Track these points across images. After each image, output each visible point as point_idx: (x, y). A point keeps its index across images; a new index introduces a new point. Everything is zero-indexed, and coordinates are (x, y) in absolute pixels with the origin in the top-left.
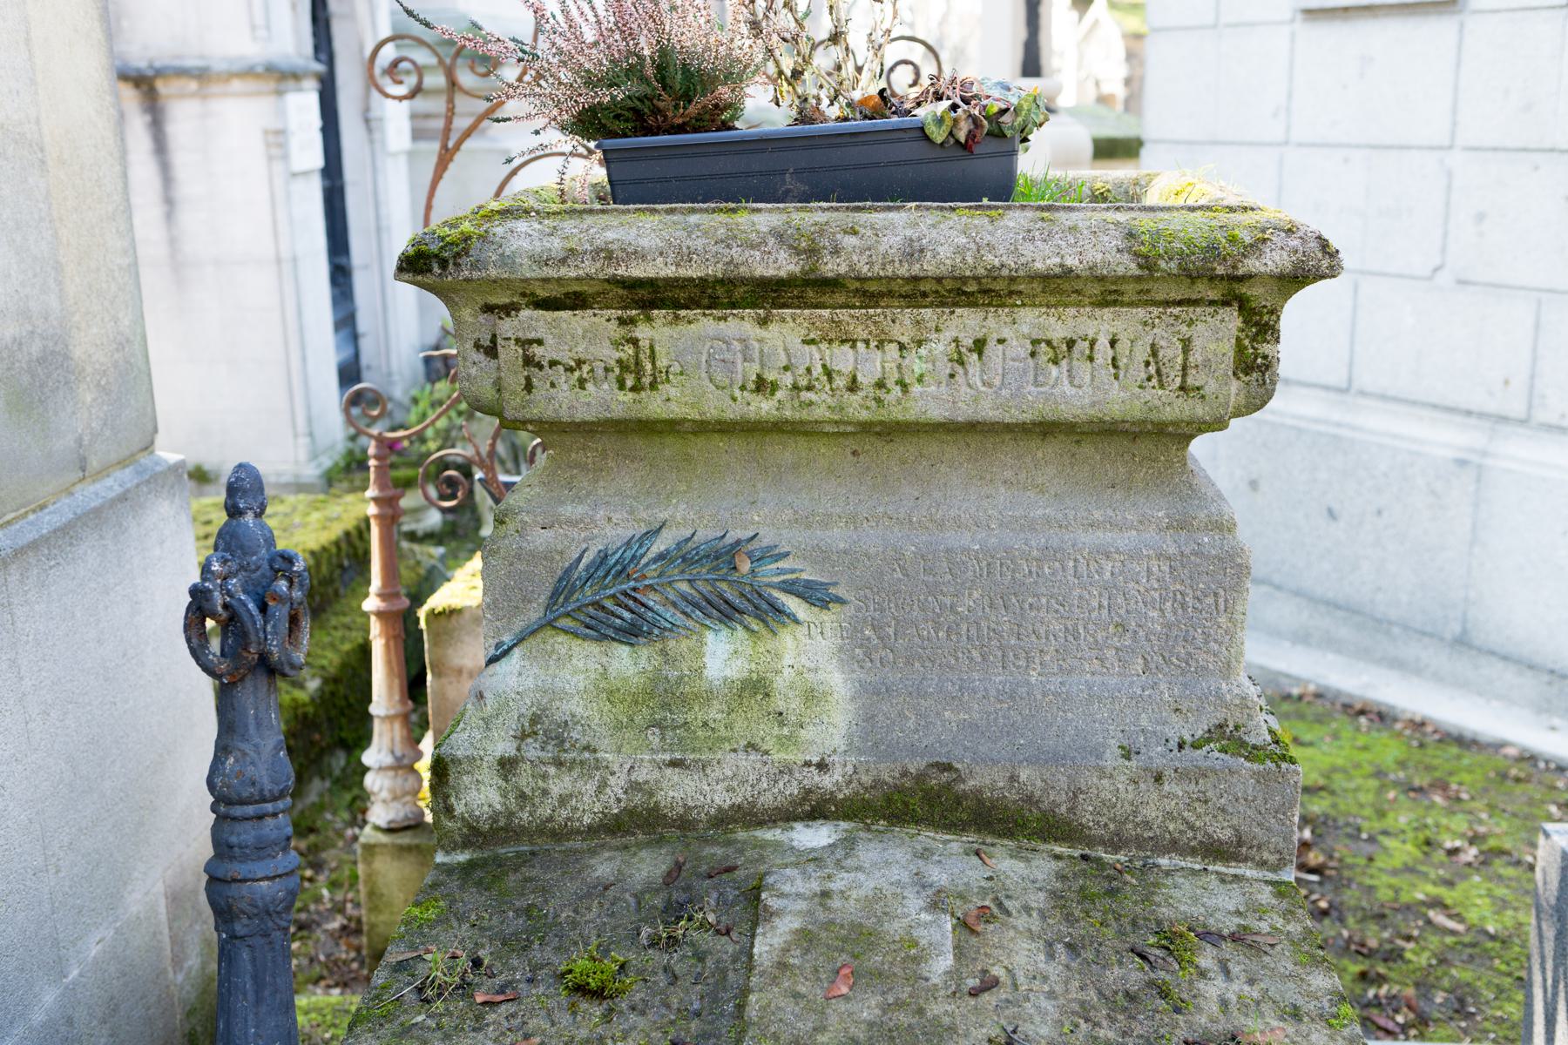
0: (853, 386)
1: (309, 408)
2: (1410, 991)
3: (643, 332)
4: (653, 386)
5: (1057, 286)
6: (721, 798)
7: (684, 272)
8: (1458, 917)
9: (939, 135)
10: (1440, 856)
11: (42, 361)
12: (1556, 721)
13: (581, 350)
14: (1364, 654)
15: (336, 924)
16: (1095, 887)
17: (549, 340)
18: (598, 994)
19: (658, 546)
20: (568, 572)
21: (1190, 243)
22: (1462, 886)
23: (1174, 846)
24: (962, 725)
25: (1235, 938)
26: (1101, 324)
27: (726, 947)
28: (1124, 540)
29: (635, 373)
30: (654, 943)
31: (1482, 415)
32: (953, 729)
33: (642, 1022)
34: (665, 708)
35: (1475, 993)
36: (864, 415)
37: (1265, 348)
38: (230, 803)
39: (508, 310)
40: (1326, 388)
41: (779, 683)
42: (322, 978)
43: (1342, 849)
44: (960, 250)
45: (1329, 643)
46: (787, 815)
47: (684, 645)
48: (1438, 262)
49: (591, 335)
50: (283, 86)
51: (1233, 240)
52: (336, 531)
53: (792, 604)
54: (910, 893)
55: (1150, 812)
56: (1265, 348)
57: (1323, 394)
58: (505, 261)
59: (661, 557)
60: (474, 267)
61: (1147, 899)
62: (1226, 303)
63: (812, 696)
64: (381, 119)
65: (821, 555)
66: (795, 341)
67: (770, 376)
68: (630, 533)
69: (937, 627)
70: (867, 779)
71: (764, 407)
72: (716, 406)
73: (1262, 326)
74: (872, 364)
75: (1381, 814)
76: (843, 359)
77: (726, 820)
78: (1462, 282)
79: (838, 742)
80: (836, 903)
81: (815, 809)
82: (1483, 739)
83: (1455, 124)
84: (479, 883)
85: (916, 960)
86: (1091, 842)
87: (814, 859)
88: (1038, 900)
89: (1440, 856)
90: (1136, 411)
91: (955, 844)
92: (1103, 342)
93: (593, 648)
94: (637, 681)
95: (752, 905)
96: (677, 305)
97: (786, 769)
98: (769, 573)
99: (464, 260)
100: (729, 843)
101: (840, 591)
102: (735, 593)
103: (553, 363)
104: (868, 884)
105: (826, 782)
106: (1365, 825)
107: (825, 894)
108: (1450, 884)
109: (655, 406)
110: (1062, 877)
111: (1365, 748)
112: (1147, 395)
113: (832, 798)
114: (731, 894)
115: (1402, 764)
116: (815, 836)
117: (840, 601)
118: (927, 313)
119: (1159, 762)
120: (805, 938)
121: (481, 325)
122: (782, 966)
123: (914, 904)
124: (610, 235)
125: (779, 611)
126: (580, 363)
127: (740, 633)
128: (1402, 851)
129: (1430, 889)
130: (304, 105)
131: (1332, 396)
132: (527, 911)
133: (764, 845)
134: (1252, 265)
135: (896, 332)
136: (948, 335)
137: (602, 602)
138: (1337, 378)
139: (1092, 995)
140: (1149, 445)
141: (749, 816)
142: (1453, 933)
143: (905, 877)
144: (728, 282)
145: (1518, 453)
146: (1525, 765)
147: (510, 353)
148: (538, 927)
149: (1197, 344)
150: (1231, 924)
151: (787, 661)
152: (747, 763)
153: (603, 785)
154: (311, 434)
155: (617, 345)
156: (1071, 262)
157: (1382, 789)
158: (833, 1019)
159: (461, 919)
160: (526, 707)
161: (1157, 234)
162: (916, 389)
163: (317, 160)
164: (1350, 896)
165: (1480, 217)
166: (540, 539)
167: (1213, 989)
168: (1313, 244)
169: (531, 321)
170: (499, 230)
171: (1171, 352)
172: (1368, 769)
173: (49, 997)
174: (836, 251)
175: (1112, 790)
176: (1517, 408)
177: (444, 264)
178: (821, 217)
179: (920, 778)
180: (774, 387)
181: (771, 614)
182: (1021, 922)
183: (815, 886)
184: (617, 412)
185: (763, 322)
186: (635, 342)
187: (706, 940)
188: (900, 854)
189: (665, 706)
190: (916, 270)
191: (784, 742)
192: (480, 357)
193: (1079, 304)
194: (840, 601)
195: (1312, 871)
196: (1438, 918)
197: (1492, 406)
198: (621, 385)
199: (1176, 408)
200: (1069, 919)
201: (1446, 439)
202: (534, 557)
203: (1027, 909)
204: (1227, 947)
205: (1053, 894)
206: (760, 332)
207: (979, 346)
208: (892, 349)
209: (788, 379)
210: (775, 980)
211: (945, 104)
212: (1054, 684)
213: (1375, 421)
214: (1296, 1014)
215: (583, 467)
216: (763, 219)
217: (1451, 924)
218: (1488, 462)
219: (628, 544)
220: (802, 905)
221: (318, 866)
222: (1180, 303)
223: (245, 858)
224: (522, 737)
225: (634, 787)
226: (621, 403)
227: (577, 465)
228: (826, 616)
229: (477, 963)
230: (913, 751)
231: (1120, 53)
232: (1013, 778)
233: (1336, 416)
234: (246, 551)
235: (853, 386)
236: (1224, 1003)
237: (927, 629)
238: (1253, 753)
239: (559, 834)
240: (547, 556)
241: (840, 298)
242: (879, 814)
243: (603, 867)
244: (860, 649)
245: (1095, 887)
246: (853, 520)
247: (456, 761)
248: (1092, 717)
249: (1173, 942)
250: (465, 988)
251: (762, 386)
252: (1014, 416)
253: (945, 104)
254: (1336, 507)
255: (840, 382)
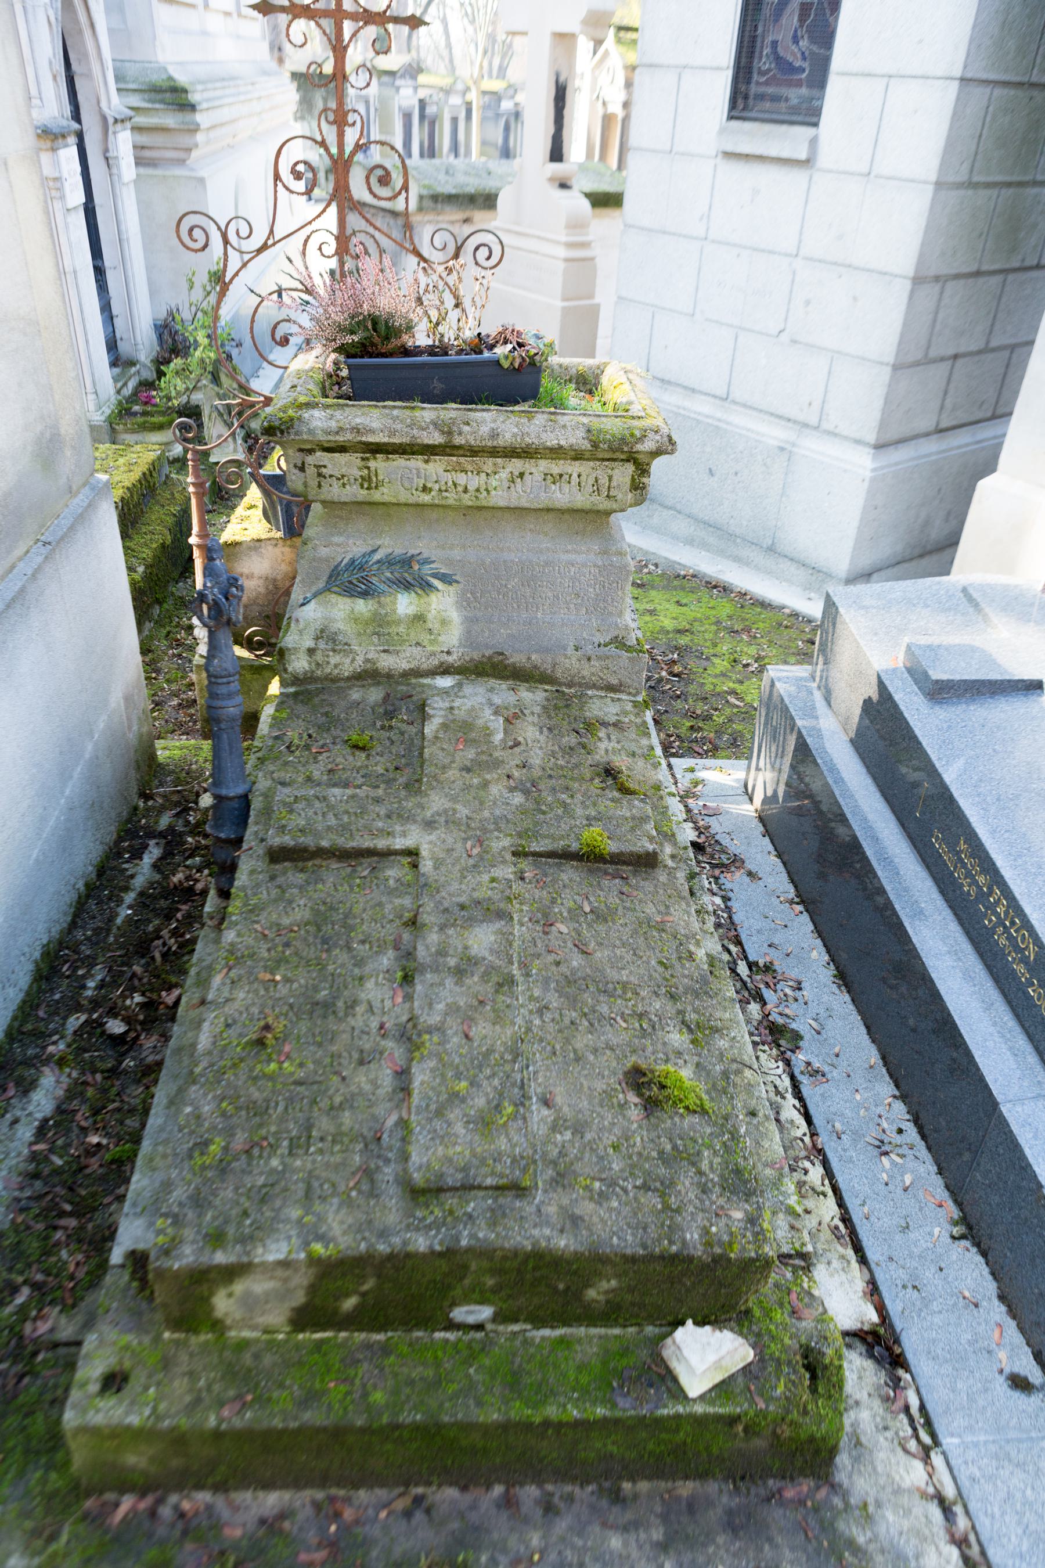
0: (466, 490)
1: (93, 375)
2: (712, 735)
3: (372, 464)
4: (376, 487)
5: (556, 453)
6: (405, 666)
7: (392, 440)
8: (741, 699)
9: (506, 364)
10: (740, 667)
11: (51, 440)
12: (812, 595)
13: (344, 471)
14: (721, 553)
15: (175, 702)
16: (561, 704)
17: (329, 466)
18: (363, 749)
19: (377, 557)
20: (336, 567)
21: (613, 436)
22: (747, 683)
23: (594, 686)
24: (509, 635)
25: (615, 725)
26: (575, 468)
27: (413, 730)
28: (580, 558)
29: (368, 481)
30: (383, 728)
31: (795, 422)
32: (503, 637)
33: (382, 760)
34: (379, 626)
35: (742, 736)
36: (470, 503)
37: (644, 480)
38: (216, 677)
39: (310, 451)
40: (715, 397)
41: (430, 616)
42: (174, 731)
43: (692, 663)
44: (515, 435)
45: (704, 546)
46: (433, 673)
47: (388, 599)
48: (782, 327)
49: (348, 464)
50: (56, 145)
51: (632, 435)
52: (136, 475)
53: (436, 583)
54: (486, 708)
55: (585, 673)
56: (644, 480)
57: (712, 400)
58: (311, 432)
59: (378, 562)
60: (296, 434)
61: (581, 709)
62: (628, 461)
63: (444, 622)
64: (116, 158)
65: (449, 562)
66: (441, 471)
67: (429, 485)
68: (364, 550)
69: (499, 593)
70: (467, 658)
71: (426, 498)
72: (404, 497)
73: (643, 469)
74: (474, 482)
75: (715, 645)
76: (461, 479)
77: (406, 674)
78: (794, 342)
79: (456, 642)
80: (456, 712)
81: (445, 670)
82: (774, 604)
83: (800, 242)
84: (302, 701)
85: (489, 735)
86: (560, 684)
87: (445, 692)
88: (537, 709)
89: (740, 667)
90: (588, 506)
91: (504, 685)
92: (575, 475)
93: (348, 600)
94: (367, 615)
95: (422, 711)
96: (388, 452)
97: (433, 654)
98: (427, 569)
99: (292, 431)
100: (409, 684)
101: (457, 578)
102: (409, 575)
103: (331, 476)
104: (469, 704)
105: (450, 659)
106: (706, 651)
107: (452, 708)
108: (741, 682)
109: (377, 496)
110: (547, 700)
111: (713, 608)
112: (592, 499)
113: (452, 666)
114: (412, 707)
115: (730, 617)
116: (445, 682)
117: (457, 582)
118: (499, 460)
119: (590, 653)
120: (445, 726)
121: (298, 458)
122: (436, 738)
123: (488, 712)
124: (358, 420)
125: (430, 585)
126: (343, 476)
127: (413, 594)
128: (721, 665)
129: (731, 685)
130: (69, 154)
131: (717, 401)
132: (326, 714)
133: (423, 685)
134: (639, 447)
135: (485, 468)
136: (508, 470)
137: (352, 580)
138: (721, 392)
139: (556, 748)
140: (593, 520)
141: (417, 673)
142: (738, 707)
143: (484, 701)
144: (411, 445)
145: (812, 446)
146: (792, 619)
147: (311, 471)
148: (329, 723)
149: (615, 478)
150: (613, 719)
151: (433, 606)
152: (416, 651)
153: (353, 660)
154: (96, 393)
155: (360, 469)
156: (563, 443)
157: (716, 633)
158: (458, 758)
159: (298, 717)
160: (318, 625)
161: (600, 431)
162: (493, 493)
163: (79, 197)
164: (692, 688)
165: (808, 303)
166: (324, 552)
167: (603, 745)
168: (666, 439)
169: (320, 457)
170: (306, 415)
171: (604, 481)
172: (714, 620)
173: (90, 747)
174: (460, 434)
175: (570, 663)
176: (813, 421)
177: (282, 432)
178: (453, 414)
179: (490, 658)
180: (431, 490)
181: (426, 587)
182: (530, 719)
183: (447, 705)
184: (360, 499)
185: (427, 462)
186: (368, 468)
187: (404, 727)
188: (481, 690)
189: (380, 626)
190: (495, 443)
191: (432, 642)
192: (297, 471)
193: (565, 459)
194: (457, 582)
195: (675, 676)
196: (732, 700)
197: (801, 417)
198: (362, 487)
199: (605, 505)
200: (549, 717)
201: (775, 434)
202: (321, 560)
203: (533, 713)
204: (611, 728)
205: (544, 707)
206: (424, 466)
207: (521, 475)
208: (483, 475)
209: (437, 487)
210: (434, 744)
211: (509, 347)
212: (547, 619)
213: (740, 420)
214: (634, 755)
215: (341, 518)
216: (427, 412)
217: (737, 703)
218: (795, 450)
219: (364, 556)
220: (442, 713)
221: (158, 671)
222: (608, 460)
223: (223, 699)
224: (317, 639)
225: (367, 661)
226: (362, 494)
227: (338, 517)
228: (451, 588)
229: (310, 736)
230: (487, 646)
231: (621, 81)
232: (529, 658)
233: (719, 415)
234: (218, 576)
235: (466, 490)
236: (607, 751)
237: (494, 594)
238: (629, 649)
239: (335, 680)
240: (327, 560)
241: (461, 452)
242: (472, 672)
243: (355, 695)
244: (464, 602)
245: (561, 704)
246: (464, 547)
247: (288, 649)
248: (563, 628)
249: (590, 727)
250: (307, 747)
251: (425, 489)
252: (536, 506)
253: (509, 347)
254: (714, 469)
255: (460, 489)
